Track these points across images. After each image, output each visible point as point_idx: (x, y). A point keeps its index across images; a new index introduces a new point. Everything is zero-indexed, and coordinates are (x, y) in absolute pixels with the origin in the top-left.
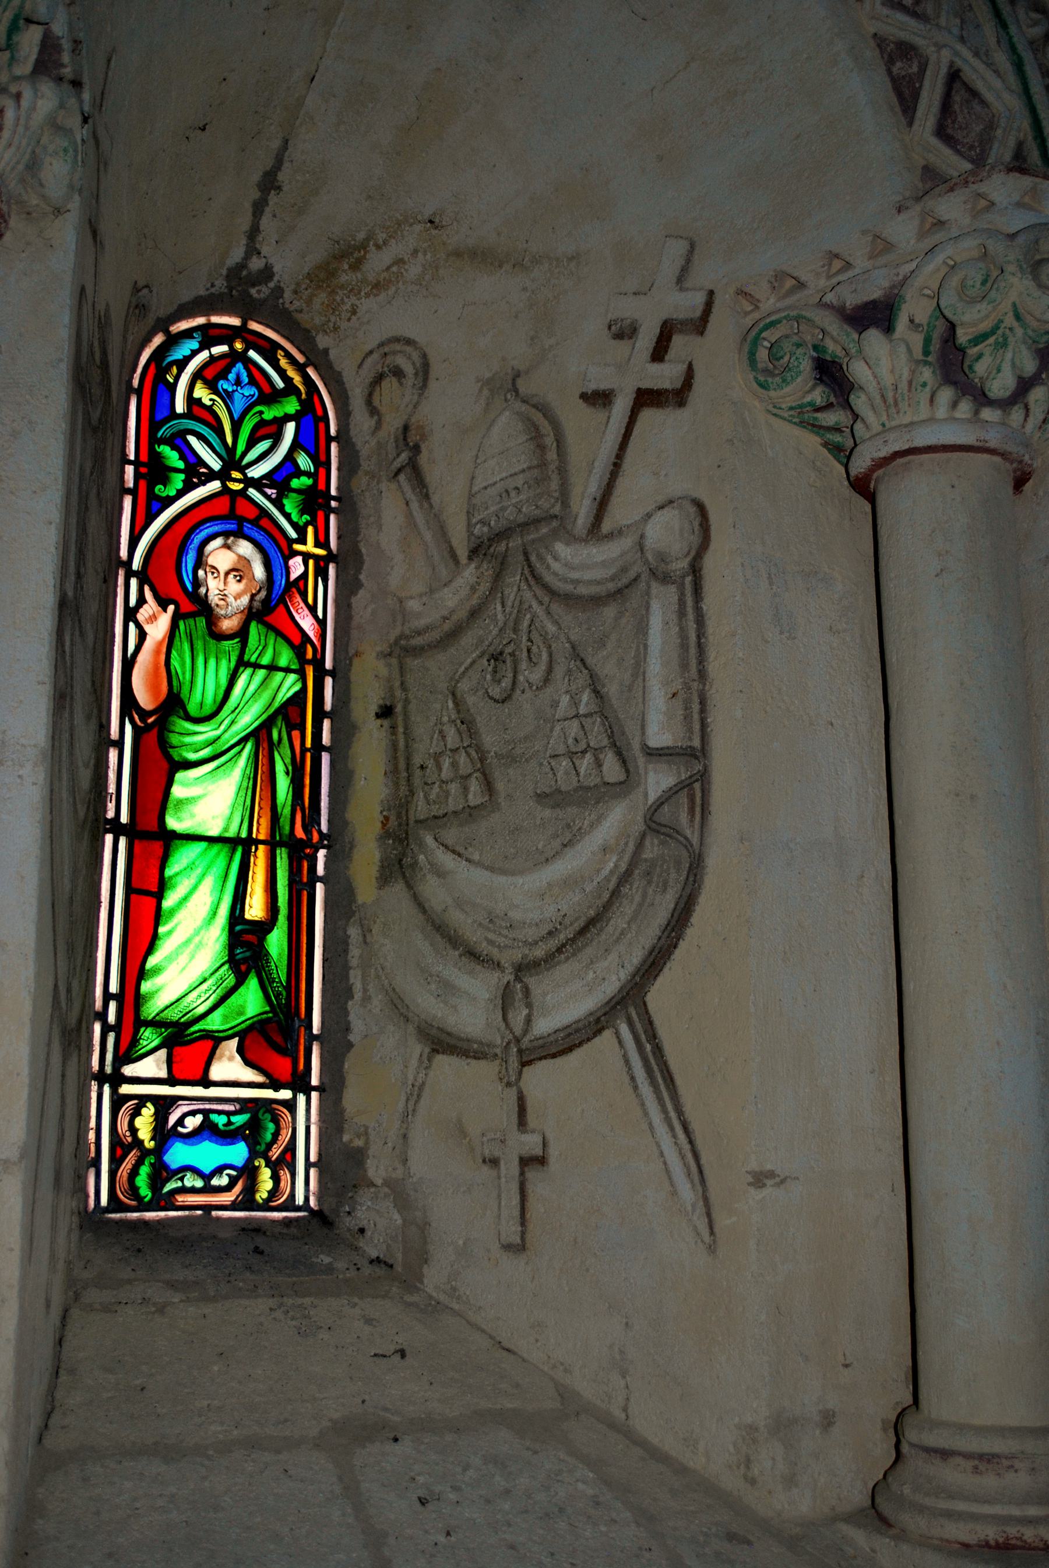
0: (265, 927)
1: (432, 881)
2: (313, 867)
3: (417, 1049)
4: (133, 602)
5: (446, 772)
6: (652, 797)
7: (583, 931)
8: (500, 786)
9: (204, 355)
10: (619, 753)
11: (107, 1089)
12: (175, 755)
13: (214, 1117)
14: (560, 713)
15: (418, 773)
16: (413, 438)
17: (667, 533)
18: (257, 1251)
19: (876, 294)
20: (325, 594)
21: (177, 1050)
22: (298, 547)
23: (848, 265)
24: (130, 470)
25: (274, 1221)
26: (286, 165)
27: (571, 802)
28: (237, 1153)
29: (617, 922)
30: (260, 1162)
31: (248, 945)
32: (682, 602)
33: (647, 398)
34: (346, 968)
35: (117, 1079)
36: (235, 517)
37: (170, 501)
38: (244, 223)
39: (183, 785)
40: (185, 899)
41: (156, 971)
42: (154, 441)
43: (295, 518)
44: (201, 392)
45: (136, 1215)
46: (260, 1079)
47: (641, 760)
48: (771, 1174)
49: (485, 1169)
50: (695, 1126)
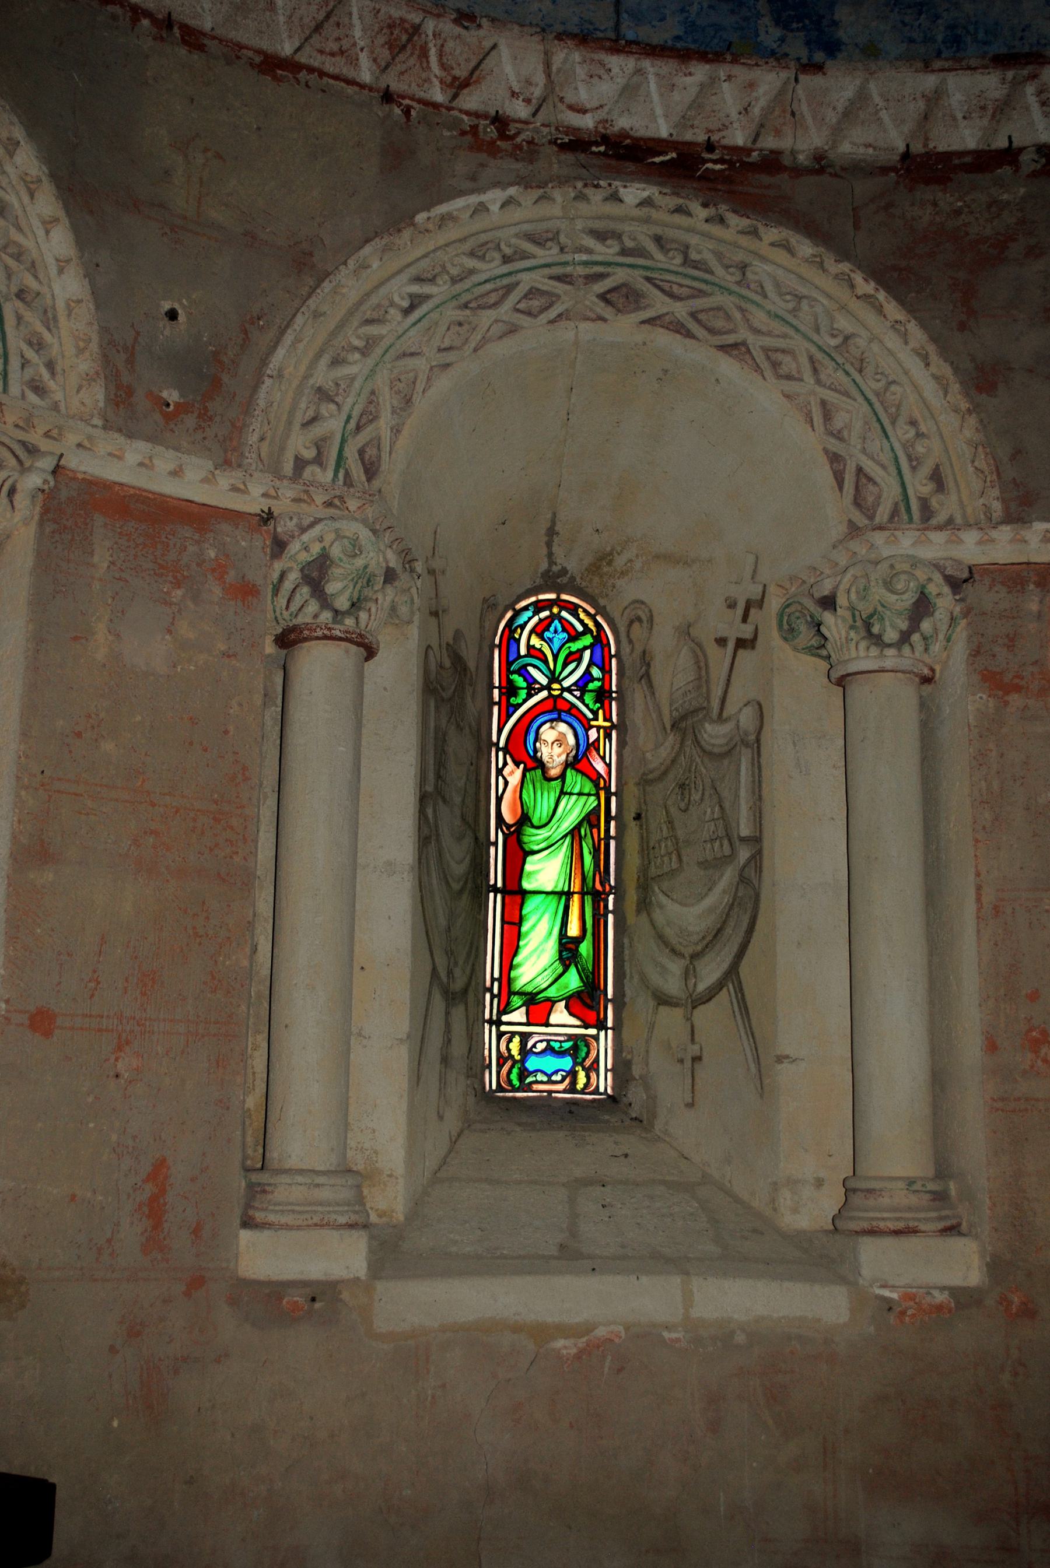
0: (578, 940)
1: (658, 911)
2: (606, 906)
3: (652, 1003)
4: (500, 766)
5: (663, 852)
6: (742, 863)
7: (716, 936)
8: (684, 859)
9: (536, 619)
10: (729, 840)
11: (494, 1028)
12: (527, 848)
13: (552, 1043)
14: (707, 818)
15: (652, 852)
16: (647, 659)
17: (747, 719)
18: (570, 1112)
19: (826, 593)
20: (611, 748)
21: (531, 1007)
22: (593, 723)
23: (822, 573)
24: (496, 692)
25: (585, 1100)
26: (558, 523)
27: (713, 865)
28: (567, 1063)
29: (728, 931)
30: (579, 1068)
31: (570, 950)
32: (753, 759)
33: (741, 644)
34: (623, 961)
35: (499, 1023)
36: (556, 709)
37: (520, 705)
38: (544, 551)
39: (531, 864)
40: (534, 926)
41: (518, 966)
42: (510, 672)
43: (591, 706)
44: (535, 641)
45: (511, 1094)
46: (578, 1023)
47: (737, 843)
48: (787, 1057)
49: (678, 1065)
50: (756, 1035)
